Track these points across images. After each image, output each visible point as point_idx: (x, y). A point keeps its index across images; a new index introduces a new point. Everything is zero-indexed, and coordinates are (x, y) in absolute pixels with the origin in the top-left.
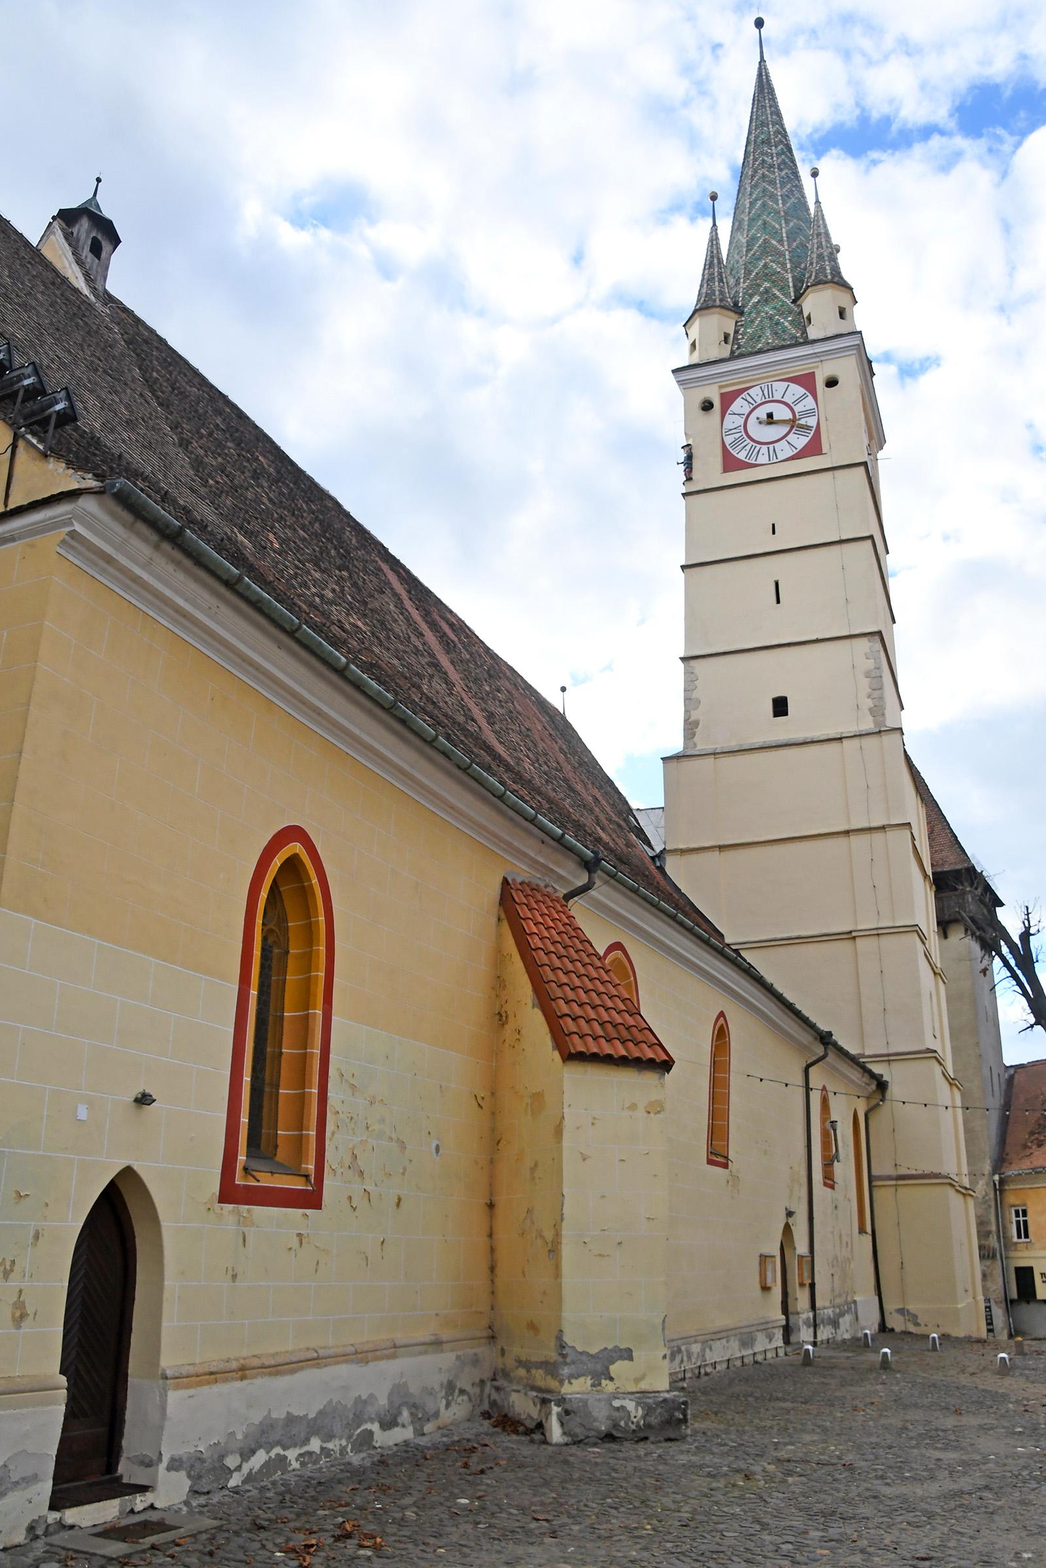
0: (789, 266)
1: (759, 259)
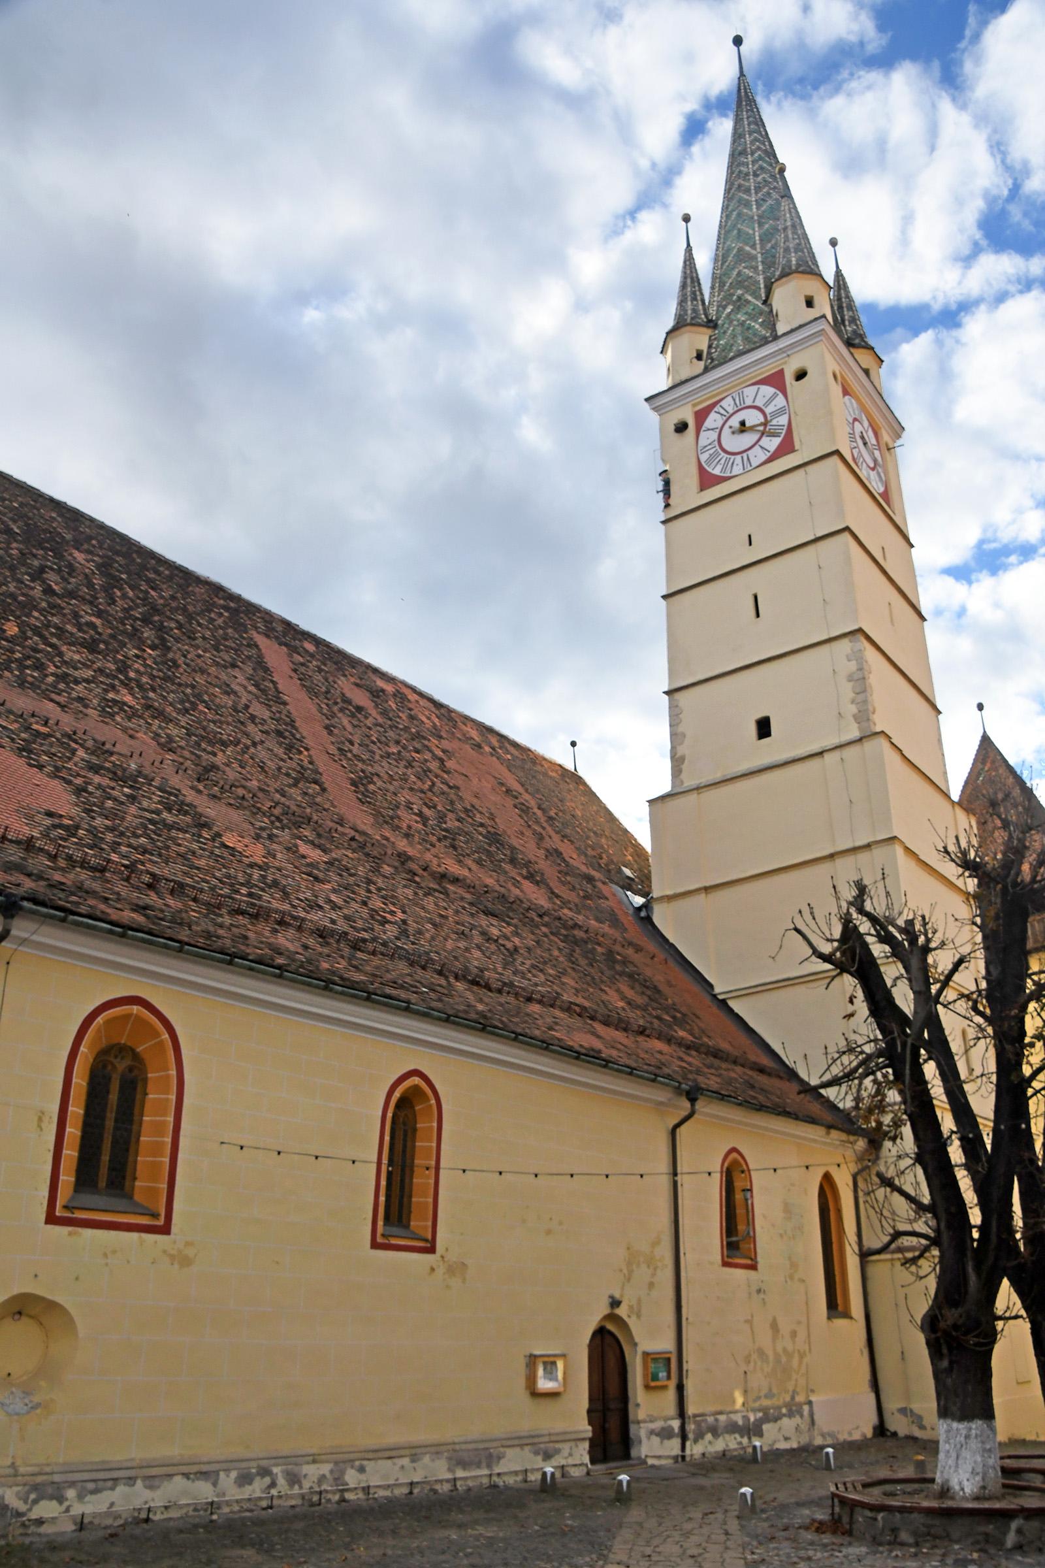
0: (760, 268)
1: (733, 269)
